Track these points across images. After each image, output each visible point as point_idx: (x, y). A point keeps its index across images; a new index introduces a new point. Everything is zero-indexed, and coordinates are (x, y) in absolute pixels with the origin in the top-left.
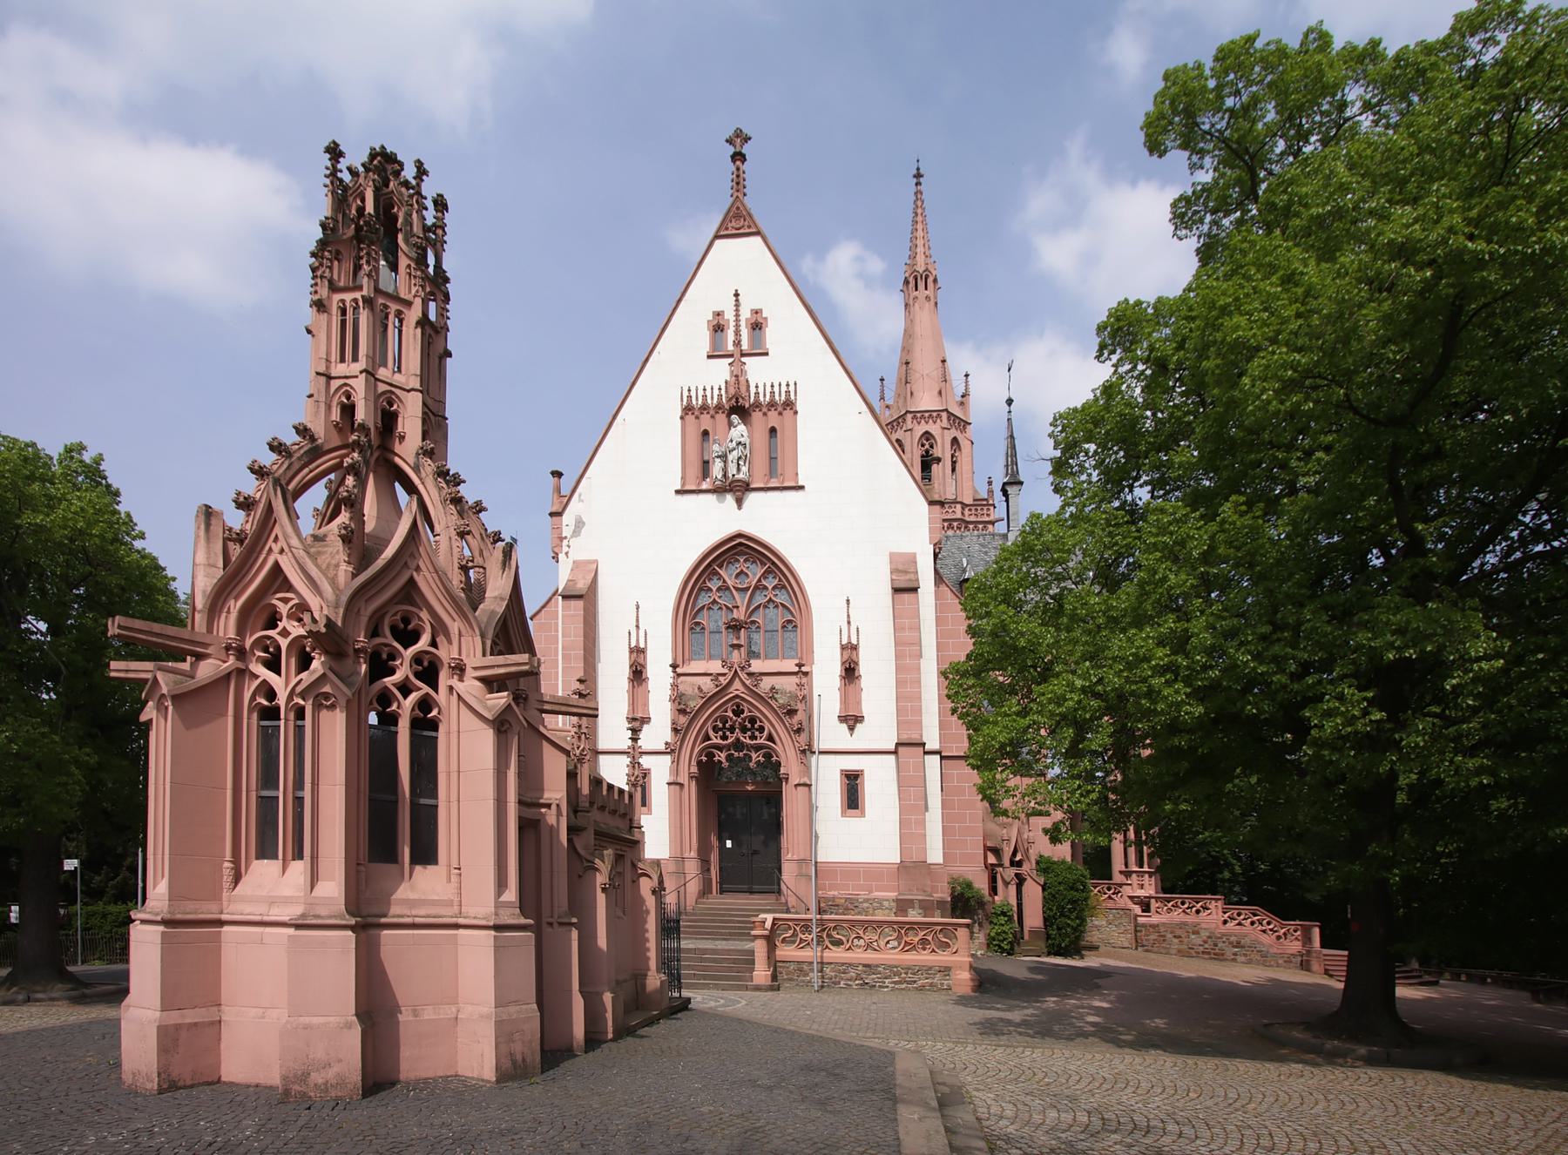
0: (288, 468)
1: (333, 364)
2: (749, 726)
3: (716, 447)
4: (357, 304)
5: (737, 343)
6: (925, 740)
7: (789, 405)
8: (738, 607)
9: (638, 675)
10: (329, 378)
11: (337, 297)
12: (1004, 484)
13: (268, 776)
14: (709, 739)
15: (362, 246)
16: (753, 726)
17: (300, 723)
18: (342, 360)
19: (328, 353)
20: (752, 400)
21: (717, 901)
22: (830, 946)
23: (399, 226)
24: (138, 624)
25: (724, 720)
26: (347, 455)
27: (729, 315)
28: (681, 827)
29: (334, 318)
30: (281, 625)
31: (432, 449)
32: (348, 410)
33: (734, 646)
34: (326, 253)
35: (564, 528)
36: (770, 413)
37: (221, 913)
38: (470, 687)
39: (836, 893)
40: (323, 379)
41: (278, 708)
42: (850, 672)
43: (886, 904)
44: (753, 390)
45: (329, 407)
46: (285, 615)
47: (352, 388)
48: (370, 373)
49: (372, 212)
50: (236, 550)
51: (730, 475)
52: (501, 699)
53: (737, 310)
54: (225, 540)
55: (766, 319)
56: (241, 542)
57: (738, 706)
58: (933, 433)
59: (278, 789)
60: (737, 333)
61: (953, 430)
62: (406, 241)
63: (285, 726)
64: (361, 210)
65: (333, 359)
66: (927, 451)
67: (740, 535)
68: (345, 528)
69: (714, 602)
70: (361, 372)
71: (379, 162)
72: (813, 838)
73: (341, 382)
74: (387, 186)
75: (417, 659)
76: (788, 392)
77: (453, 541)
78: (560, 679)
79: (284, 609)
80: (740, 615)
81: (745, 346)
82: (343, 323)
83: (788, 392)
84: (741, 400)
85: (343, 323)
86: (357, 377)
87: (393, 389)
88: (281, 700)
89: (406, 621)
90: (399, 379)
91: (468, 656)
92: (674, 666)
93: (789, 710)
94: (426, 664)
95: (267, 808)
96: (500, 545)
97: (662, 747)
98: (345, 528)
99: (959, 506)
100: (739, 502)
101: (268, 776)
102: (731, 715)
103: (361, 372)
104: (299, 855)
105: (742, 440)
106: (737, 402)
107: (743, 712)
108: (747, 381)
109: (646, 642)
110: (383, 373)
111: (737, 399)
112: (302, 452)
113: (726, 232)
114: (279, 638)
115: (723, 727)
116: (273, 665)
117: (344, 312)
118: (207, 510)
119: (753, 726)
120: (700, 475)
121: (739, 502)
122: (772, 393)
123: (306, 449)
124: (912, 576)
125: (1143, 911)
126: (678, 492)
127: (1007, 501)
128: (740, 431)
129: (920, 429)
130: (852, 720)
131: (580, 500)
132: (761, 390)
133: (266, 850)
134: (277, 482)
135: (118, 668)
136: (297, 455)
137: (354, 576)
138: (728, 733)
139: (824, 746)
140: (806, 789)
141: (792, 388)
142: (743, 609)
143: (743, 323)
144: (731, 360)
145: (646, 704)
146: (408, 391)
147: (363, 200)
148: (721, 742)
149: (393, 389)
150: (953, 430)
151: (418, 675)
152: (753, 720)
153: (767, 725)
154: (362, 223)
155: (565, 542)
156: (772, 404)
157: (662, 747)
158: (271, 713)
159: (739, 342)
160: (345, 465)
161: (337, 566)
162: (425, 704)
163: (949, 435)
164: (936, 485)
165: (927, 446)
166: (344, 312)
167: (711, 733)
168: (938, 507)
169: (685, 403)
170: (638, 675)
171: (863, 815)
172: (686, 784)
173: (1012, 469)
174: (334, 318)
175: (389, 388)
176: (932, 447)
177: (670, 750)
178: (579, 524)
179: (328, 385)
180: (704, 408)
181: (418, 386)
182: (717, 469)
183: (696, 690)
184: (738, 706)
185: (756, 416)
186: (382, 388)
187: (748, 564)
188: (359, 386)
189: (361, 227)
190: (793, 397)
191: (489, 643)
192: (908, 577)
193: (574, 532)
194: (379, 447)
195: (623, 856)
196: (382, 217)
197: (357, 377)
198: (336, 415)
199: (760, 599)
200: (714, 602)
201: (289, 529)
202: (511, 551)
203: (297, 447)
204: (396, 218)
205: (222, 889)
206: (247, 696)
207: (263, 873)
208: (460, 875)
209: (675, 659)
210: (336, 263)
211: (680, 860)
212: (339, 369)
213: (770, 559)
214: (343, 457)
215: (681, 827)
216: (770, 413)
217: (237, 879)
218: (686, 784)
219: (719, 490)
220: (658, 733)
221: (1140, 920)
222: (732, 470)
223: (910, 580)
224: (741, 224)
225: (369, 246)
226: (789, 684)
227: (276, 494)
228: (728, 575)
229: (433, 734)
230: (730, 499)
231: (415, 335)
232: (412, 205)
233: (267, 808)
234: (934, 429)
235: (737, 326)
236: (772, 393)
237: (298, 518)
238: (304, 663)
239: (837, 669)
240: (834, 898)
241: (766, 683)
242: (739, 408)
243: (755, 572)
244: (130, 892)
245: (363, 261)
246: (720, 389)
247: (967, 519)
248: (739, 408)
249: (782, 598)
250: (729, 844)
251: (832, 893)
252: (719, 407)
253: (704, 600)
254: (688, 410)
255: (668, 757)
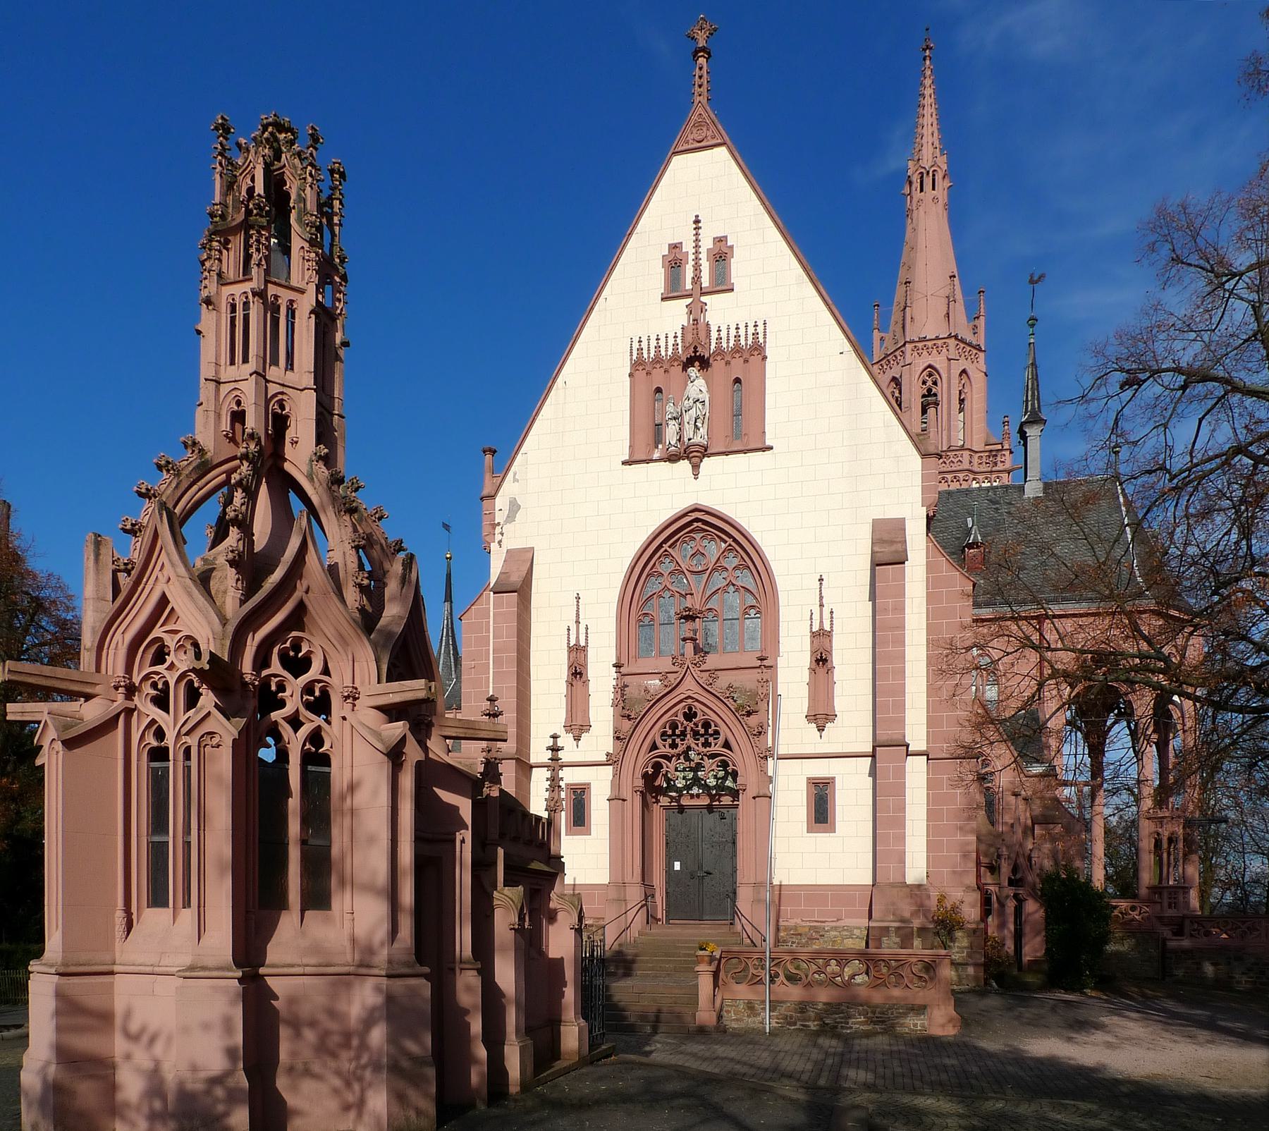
0: (177, 487)
1: (223, 368)
2: (702, 731)
3: (670, 408)
4: (247, 298)
5: (697, 279)
6: (908, 740)
7: (758, 350)
8: (692, 594)
9: (577, 673)
10: (218, 382)
11: (227, 290)
12: (1022, 424)
13: (159, 821)
14: (657, 748)
15: (251, 232)
16: (706, 731)
17: (187, 763)
18: (232, 363)
19: (218, 356)
20: (713, 347)
21: (662, 931)
22: (786, 982)
23: (291, 205)
24: (26, 666)
25: (674, 726)
26: (234, 470)
27: (688, 247)
28: (623, 849)
29: (224, 316)
30: (169, 659)
31: (327, 454)
32: (238, 417)
33: (980, 464)
34: (215, 244)
35: (497, 513)
36: (733, 362)
37: (114, 964)
38: (366, 716)
39: (799, 921)
40: (213, 385)
41: (167, 749)
42: (821, 660)
43: (857, 932)
44: (714, 335)
45: (218, 416)
46: (172, 649)
47: (243, 392)
48: (260, 374)
49: (262, 193)
50: (125, 581)
51: (686, 440)
52: (399, 728)
53: (697, 240)
54: (115, 572)
55: (732, 247)
56: (129, 572)
57: (690, 709)
58: (937, 366)
59: (168, 833)
60: (697, 267)
61: (963, 360)
62: (299, 220)
63: (174, 767)
64: (251, 191)
65: (223, 362)
66: (929, 390)
67: (696, 510)
68: (232, 551)
69: (666, 588)
70: (251, 375)
71: (271, 133)
72: (765, 860)
73: (232, 385)
74: (279, 160)
75: (308, 689)
76: (755, 334)
77: (347, 555)
78: (491, 685)
79: (171, 642)
80: (694, 603)
81: (705, 282)
82: (233, 320)
83: (755, 334)
84: (699, 349)
85: (233, 320)
86: (247, 380)
87: (285, 390)
88: (170, 740)
89: (296, 646)
90: (290, 378)
91: (362, 683)
92: (618, 666)
93: (748, 712)
94: (317, 693)
95: (158, 854)
96: (402, 555)
97: (604, 758)
98: (232, 551)
99: (966, 453)
100: (696, 467)
101: (159, 821)
102: (682, 719)
103: (251, 375)
104: (187, 904)
105: (700, 397)
106: (695, 352)
107: (695, 715)
108: (708, 324)
109: (587, 640)
110: (274, 373)
111: (695, 348)
112: (191, 468)
113: (686, 147)
114: (166, 673)
115: (673, 733)
116: (161, 701)
117: (233, 308)
118: (96, 539)
119: (706, 731)
120: (651, 442)
121: (696, 467)
122: (737, 336)
123: (194, 464)
124: (899, 547)
125: (1175, 934)
126: (624, 463)
127: (1025, 445)
128: (698, 385)
129: (921, 363)
130: (821, 717)
131: (515, 480)
132: (724, 334)
133: (158, 898)
134: (163, 506)
135: (15, 711)
136: (186, 472)
137: (242, 602)
138: (678, 741)
139: (782, 750)
140: (768, 799)
141: (760, 329)
142: (697, 597)
143: (703, 256)
144: (690, 300)
145: (586, 711)
146: (302, 390)
147: (253, 180)
148: (670, 750)
149: (285, 390)
150: (963, 360)
151: (308, 706)
152: (707, 725)
153: (723, 729)
154: (251, 206)
155: (498, 530)
156: (737, 350)
157: (604, 758)
158: (159, 754)
159: (699, 278)
160: (233, 481)
161: (225, 592)
162: (316, 738)
163: (956, 368)
164: (931, 435)
165: (929, 383)
166: (233, 308)
167: (659, 742)
168: (934, 460)
169: (634, 358)
170: (577, 673)
171: (832, 830)
172: (629, 798)
173: (1033, 405)
174: (224, 316)
175: (280, 389)
176: (935, 383)
177: (611, 760)
178: (514, 507)
179: (217, 391)
180: (658, 360)
181: (311, 384)
182: (671, 433)
183: (643, 693)
184: (690, 709)
185: (717, 365)
186: (273, 388)
187: (705, 542)
188: (249, 391)
189: (251, 211)
190: (761, 340)
191: (385, 668)
192: (893, 548)
193: (508, 517)
194: (271, 455)
195: (539, 890)
196: (273, 196)
197: (247, 380)
198: (225, 424)
199: (719, 580)
200: (666, 588)
201: (176, 557)
202: (411, 563)
203: (186, 463)
204: (288, 196)
205: (114, 937)
206: (135, 737)
207: (153, 920)
208: (353, 920)
209: (618, 658)
210: (225, 252)
211: (618, 884)
212: (228, 373)
213: (730, 536)
214: (229, 473)
215: (623, 849)
216: (733, 362)
217: (129, 926)
218: (629, 798)
219: (672, 458)
220: (600, 740)
221: (1172, 944)
222: (688, 431)
223: (896, 552)
224: (704, 135)
225: (259, 232)
226: (747, 680)
227: (161, 518)
228: (682, 554)
229: (326, 769)
230: (685, 465)
231: (308, 326)
232: (305, 179)
233: (158, 854)
234: (939, 361)
235: (697, 259)
236: (737, 336)
237: (185, 543)
238: (192, 698)
239: (805, 659)
240: (796, 928)
241: (724, 680)
242: (697, 359)
243: (713, 549)
244: (34, 941)
245: (253, 250)
246: (676, 337)
247: (976, 469)
248: (697, 359)
249: (746, 579)
250: (677, 866)
251: (795, 920)
252: (675, 358)
253: (654, 586)
254: (638, 365)
255: (611, 767)
